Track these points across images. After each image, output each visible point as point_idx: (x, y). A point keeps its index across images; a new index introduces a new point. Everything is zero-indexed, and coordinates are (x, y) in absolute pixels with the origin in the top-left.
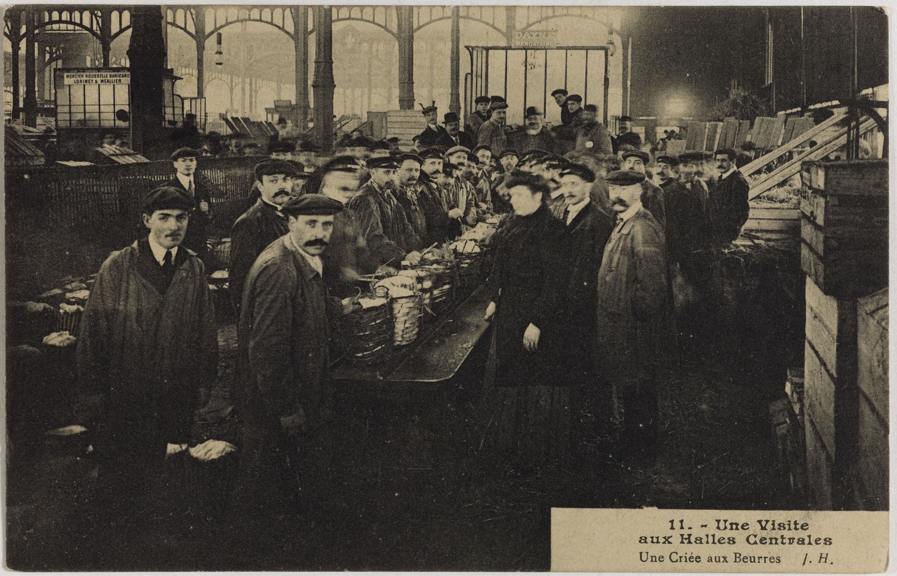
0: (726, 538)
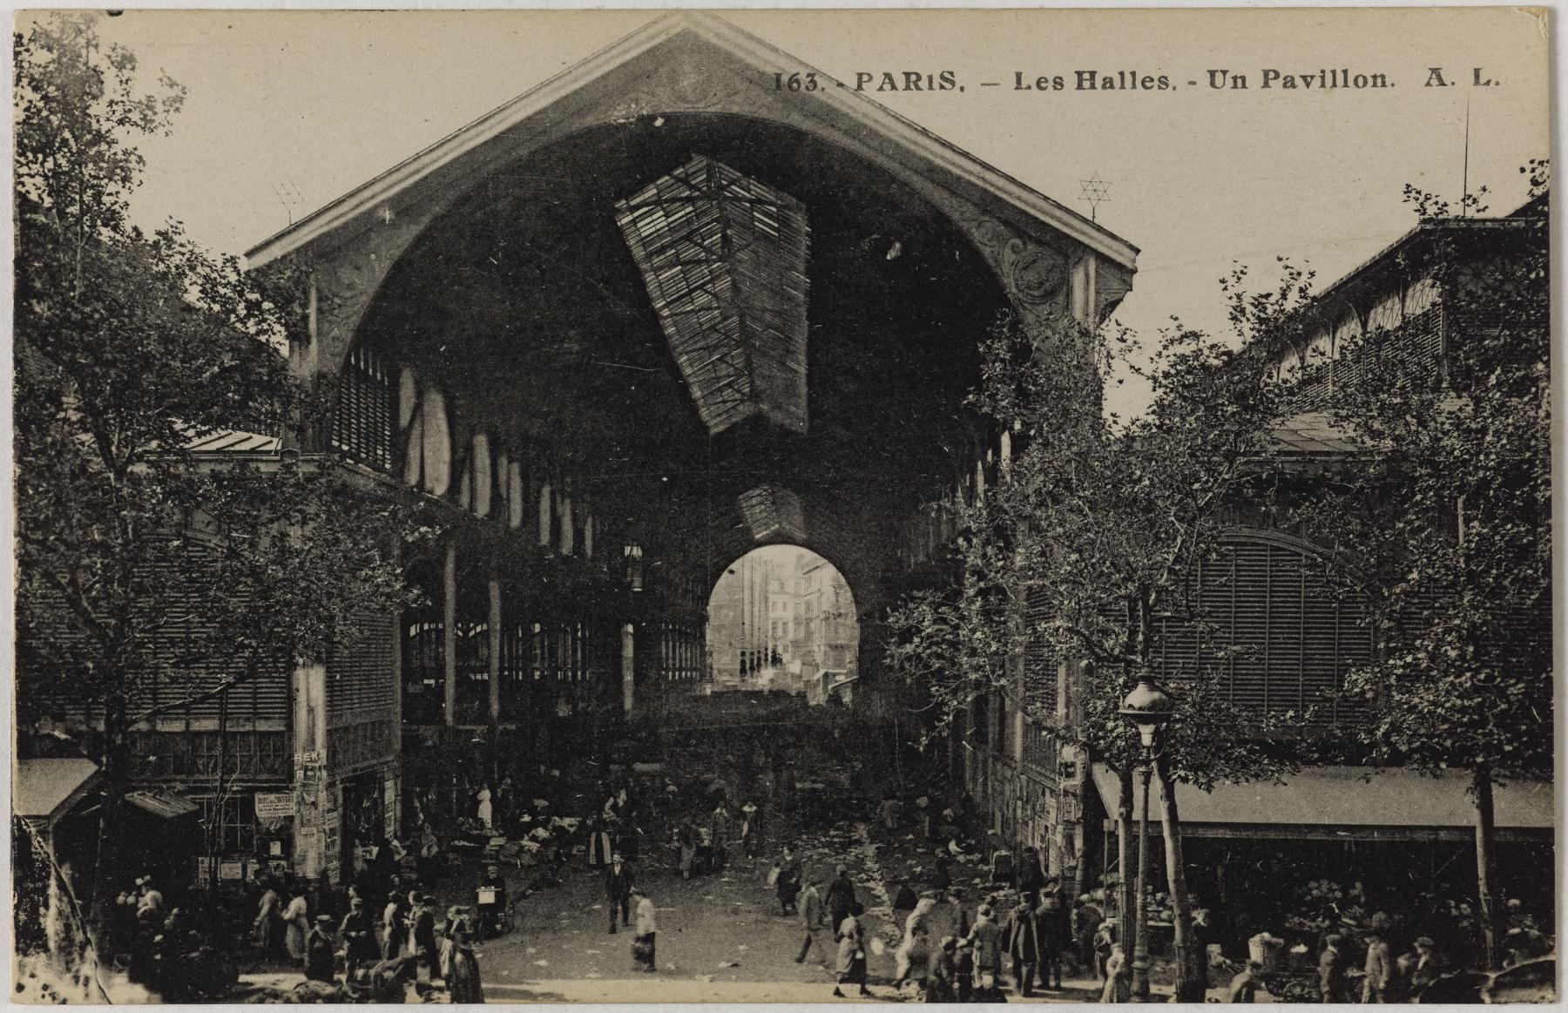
0: (1156, 79)
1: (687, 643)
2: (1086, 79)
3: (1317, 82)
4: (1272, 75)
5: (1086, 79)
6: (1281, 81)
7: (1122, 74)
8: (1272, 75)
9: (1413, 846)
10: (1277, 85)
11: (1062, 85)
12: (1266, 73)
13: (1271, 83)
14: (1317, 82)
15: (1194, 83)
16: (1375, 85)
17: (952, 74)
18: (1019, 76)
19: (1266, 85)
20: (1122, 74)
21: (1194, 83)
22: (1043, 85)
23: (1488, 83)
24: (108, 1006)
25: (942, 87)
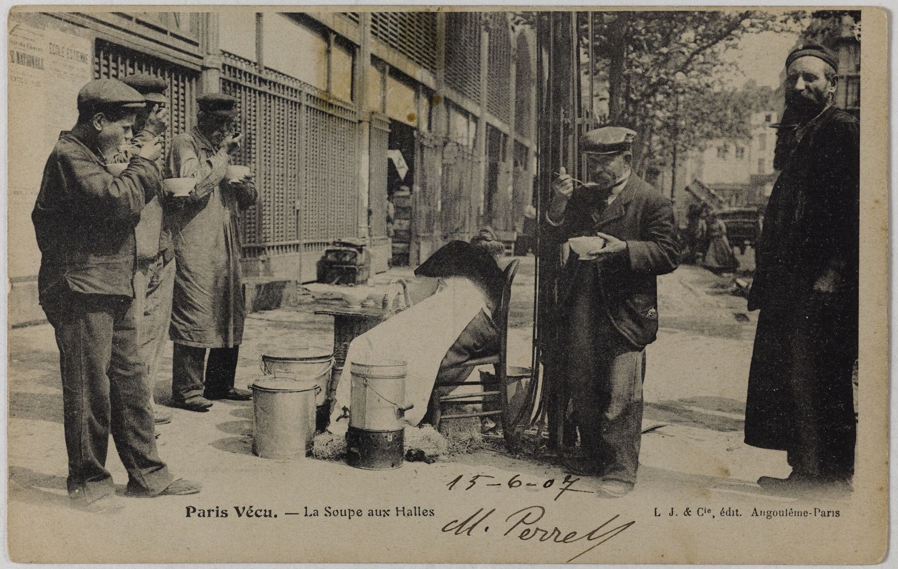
1: (190, 81)
2: (328, 512)
3: (213, 514)
4: (192, 510)
5: (328, 512)
6: (820, 513)
7: (415, 508)
8: (192, 510)
9: (852, 364)
10: (194, 516)
11: (227, 515)
12: (188, 509)
13: (191, 514)
14: (213, 514)
15: (487, 528)
16: (209, 515)
17: (326, 515)
18: (397, 508)
19: (188, 515)
20: (415, 508)
21: (487, 528)
22: (250, 514)
23: (316, 513)
24: (254, 457)
25: (222, 516)
